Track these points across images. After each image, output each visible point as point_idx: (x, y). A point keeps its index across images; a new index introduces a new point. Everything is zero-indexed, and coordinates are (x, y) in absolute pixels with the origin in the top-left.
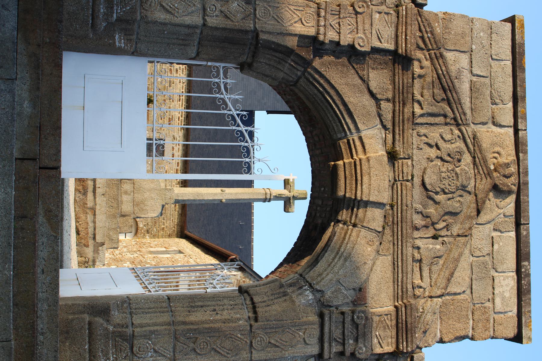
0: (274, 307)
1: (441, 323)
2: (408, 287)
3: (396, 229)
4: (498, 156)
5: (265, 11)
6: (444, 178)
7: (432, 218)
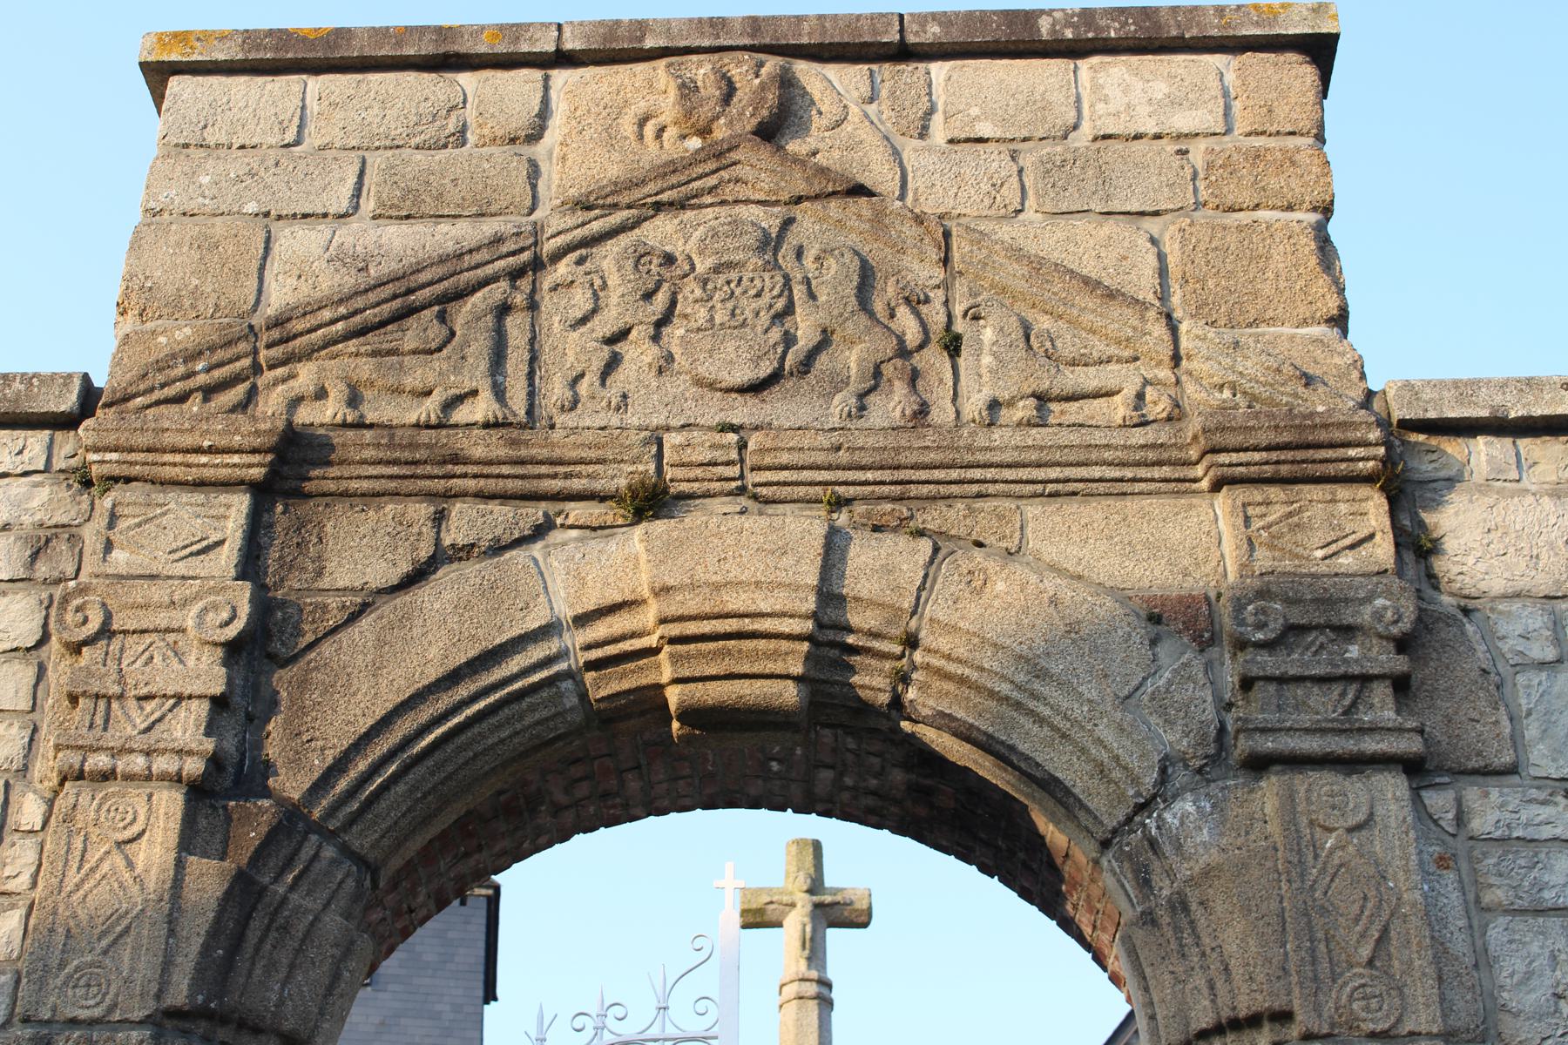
0: (1231, 948)
1: (1271, 321)
2: (1142, 442)
5: (82, 982)
6: (733, 314)
7: (880, 356)
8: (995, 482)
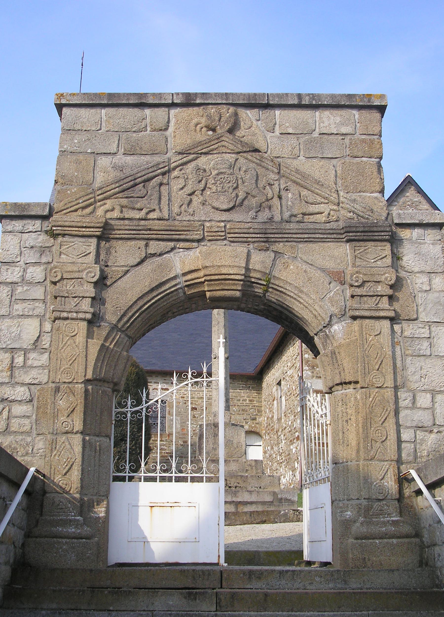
0: (345, 365)
1: (364, 192)
2: (329, 228)
3: (273, 240)
4: (199, 125)
5: (66, 373)
6: (222, 188)
7: (261, 201)
8: (291, 238)
